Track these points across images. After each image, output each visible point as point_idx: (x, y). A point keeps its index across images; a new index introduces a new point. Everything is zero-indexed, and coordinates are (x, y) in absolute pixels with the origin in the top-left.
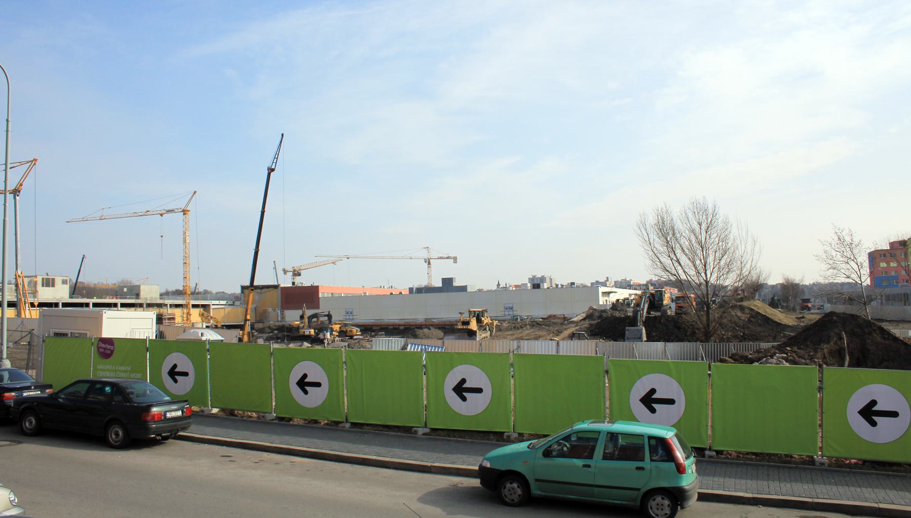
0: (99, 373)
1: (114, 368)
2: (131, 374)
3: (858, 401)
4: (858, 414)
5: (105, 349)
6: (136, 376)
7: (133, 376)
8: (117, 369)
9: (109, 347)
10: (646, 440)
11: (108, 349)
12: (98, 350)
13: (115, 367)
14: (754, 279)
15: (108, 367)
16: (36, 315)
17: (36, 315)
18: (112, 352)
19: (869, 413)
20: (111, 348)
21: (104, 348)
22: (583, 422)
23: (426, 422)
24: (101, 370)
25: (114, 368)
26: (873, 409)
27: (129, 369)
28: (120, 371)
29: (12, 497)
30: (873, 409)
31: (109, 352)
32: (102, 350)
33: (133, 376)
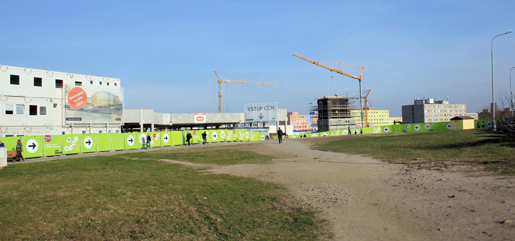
5: (48, 139)
9: (49, 138)
18: (50, 139)
20: (50, 138)
31: (49, 140)
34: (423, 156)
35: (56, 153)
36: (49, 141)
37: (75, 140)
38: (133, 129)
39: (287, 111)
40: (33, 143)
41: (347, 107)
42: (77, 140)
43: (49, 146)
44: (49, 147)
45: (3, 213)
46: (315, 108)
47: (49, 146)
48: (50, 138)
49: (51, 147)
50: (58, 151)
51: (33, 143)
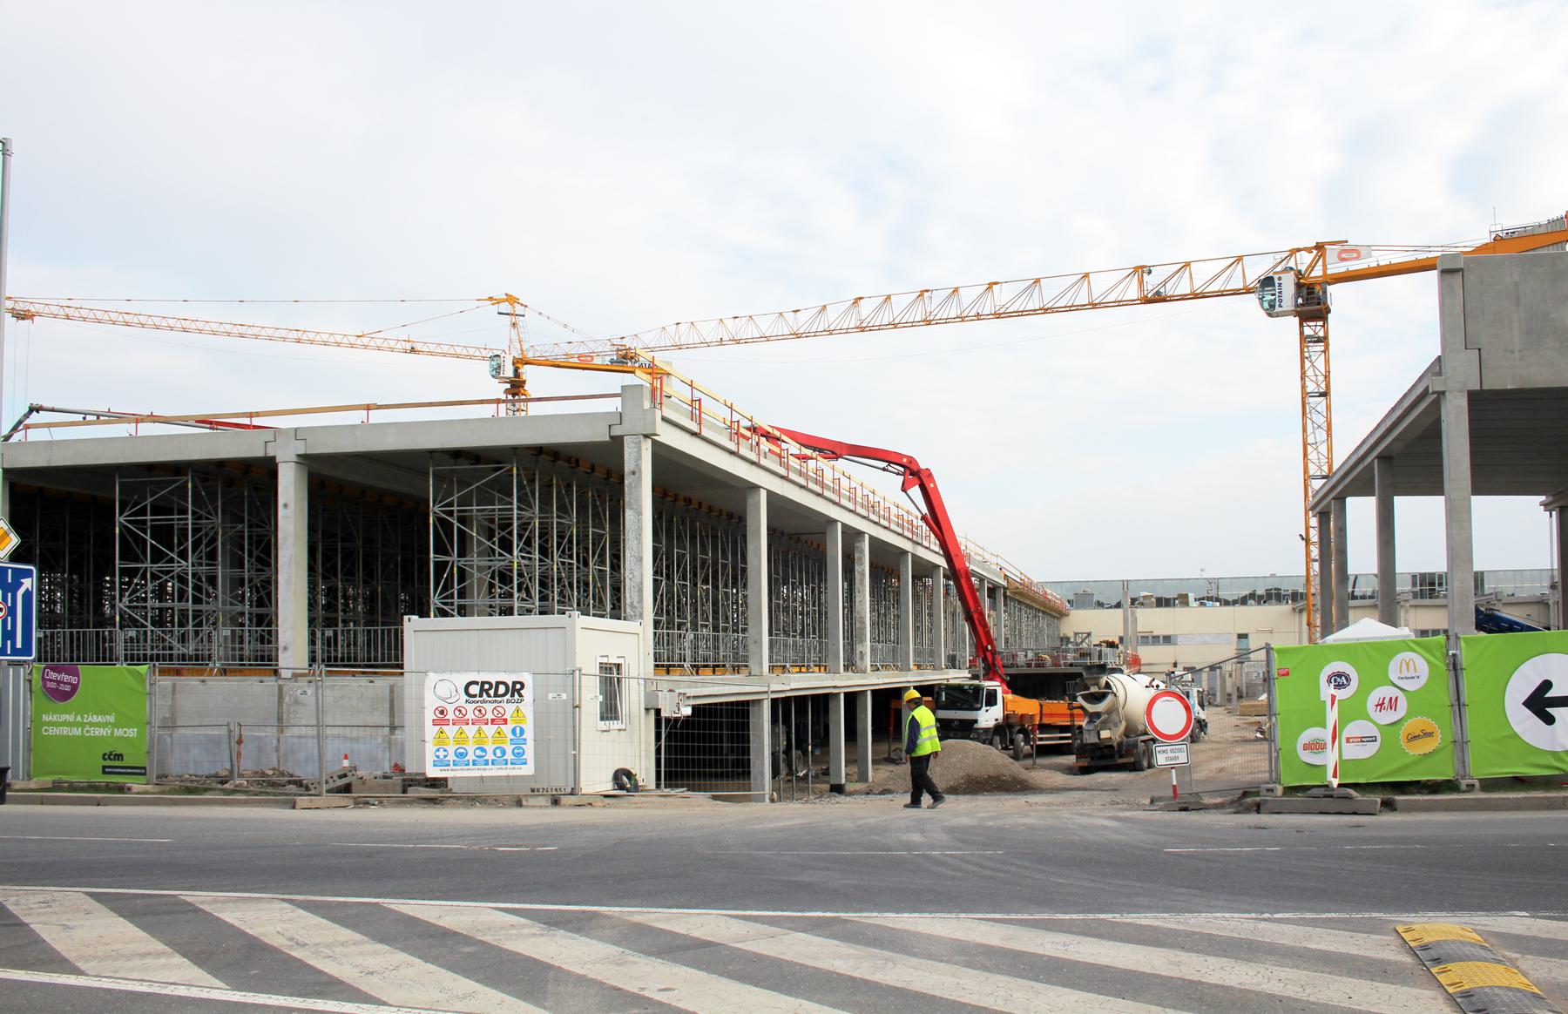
0: (88, 732)
1: (79, 718)
2: (116, 730)
3: (1522, 684)
4: (1524, 707)
5: (58, 682)
6: (125, 732)
7: (119, 733)
8: (85, 721)
9: (66, 678)
10: (591, 612)
11: (65, 683)
12: (44, 685)
13: (83, 718)
14: (1021, 659)
15: (65, 717)
16: (1051, 715)
17: (1051, 715)
18: (75, 688)
19: (1541, 703)
20: (74, 680)
21: (56, 681)
22: (363, 493)
23: (385, 1004)
24: (50, 724)
25: (79, 718)
26: (1547, 696)
27: (111, 719)
28: (92, 725)
29: (1543, 498)
30: (1547, 696)
31: (68, 688)
32: (53, 685)
33: (119, 733)
34: (423, 801)
35: (105, 770)
36: (65, 696)
37: (1393, 677)
38: (1070, 741)
39: (454, 778)
40: (1549, 720)
41: (988, 873)
42: (1423, 680)
43: (65, 724)
44: (65, 731)
45: (518, 410)
46: (627, 670)
47: (65, 724)
48: (74, 680)
49: (77, 732)
50: (119, 757)
51: (1549, 720)
